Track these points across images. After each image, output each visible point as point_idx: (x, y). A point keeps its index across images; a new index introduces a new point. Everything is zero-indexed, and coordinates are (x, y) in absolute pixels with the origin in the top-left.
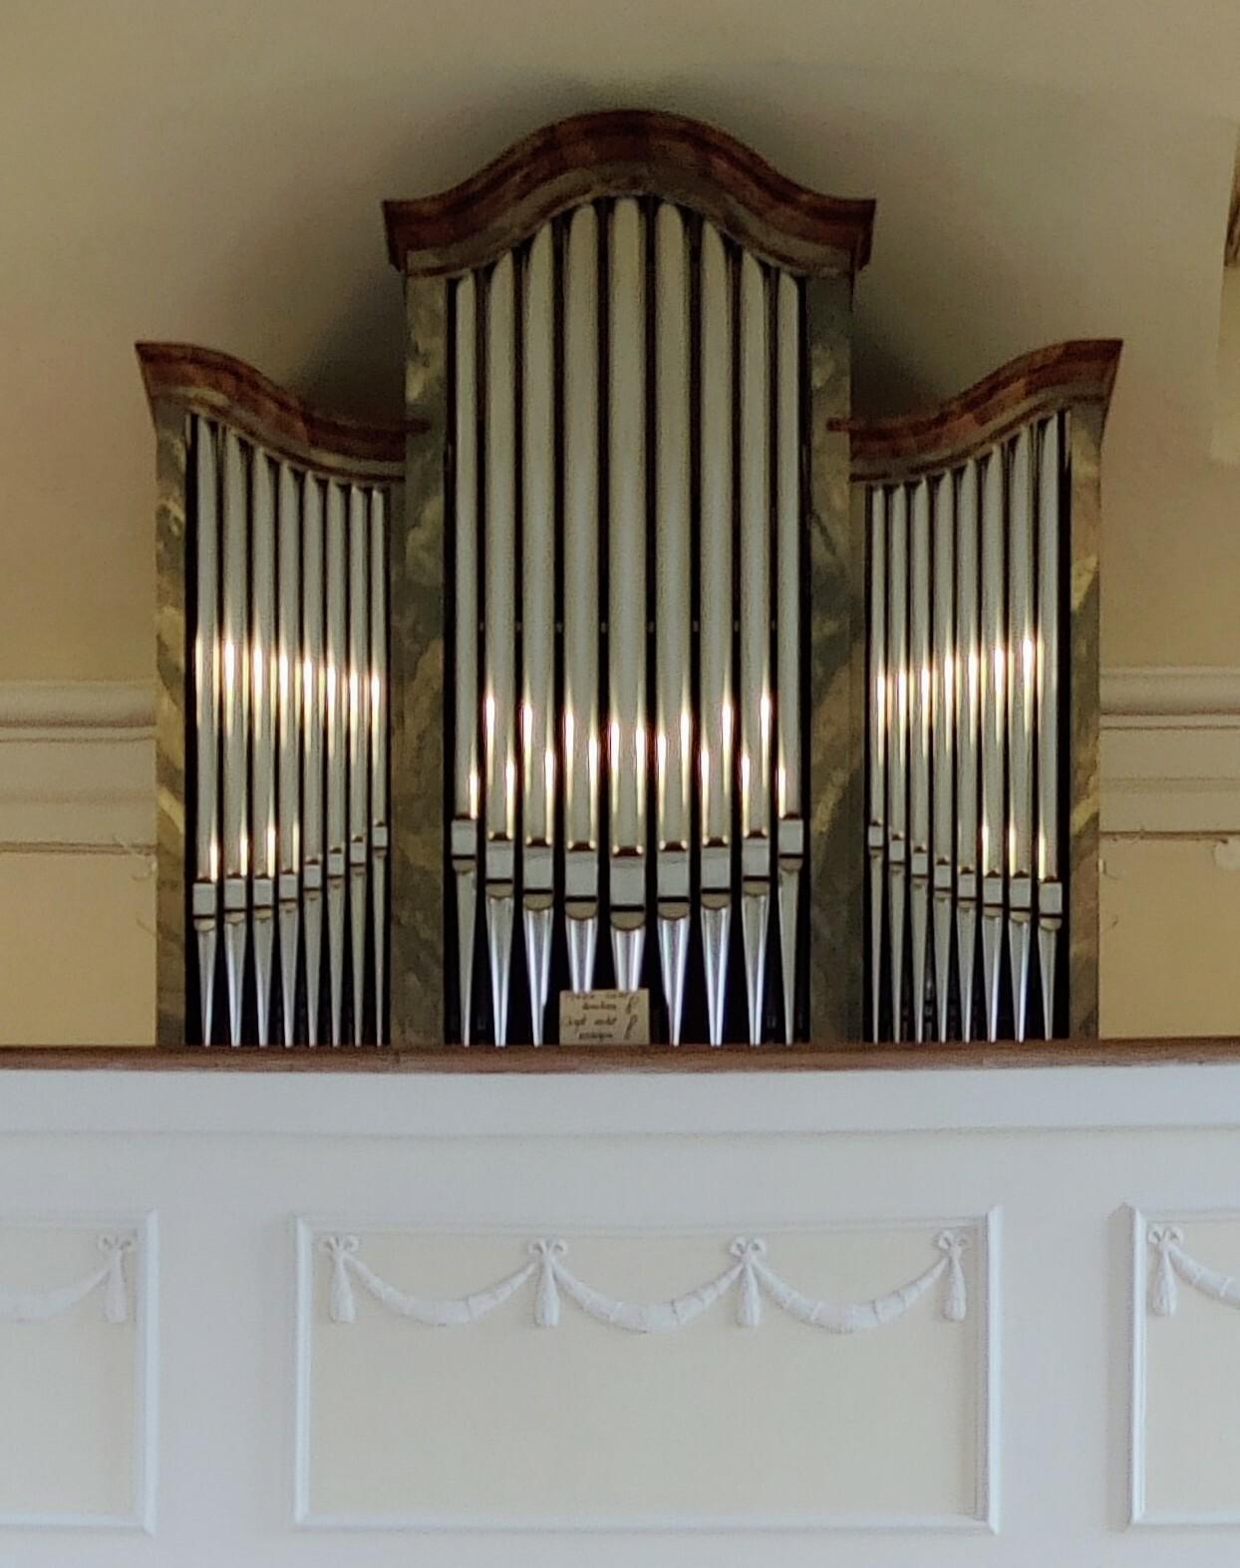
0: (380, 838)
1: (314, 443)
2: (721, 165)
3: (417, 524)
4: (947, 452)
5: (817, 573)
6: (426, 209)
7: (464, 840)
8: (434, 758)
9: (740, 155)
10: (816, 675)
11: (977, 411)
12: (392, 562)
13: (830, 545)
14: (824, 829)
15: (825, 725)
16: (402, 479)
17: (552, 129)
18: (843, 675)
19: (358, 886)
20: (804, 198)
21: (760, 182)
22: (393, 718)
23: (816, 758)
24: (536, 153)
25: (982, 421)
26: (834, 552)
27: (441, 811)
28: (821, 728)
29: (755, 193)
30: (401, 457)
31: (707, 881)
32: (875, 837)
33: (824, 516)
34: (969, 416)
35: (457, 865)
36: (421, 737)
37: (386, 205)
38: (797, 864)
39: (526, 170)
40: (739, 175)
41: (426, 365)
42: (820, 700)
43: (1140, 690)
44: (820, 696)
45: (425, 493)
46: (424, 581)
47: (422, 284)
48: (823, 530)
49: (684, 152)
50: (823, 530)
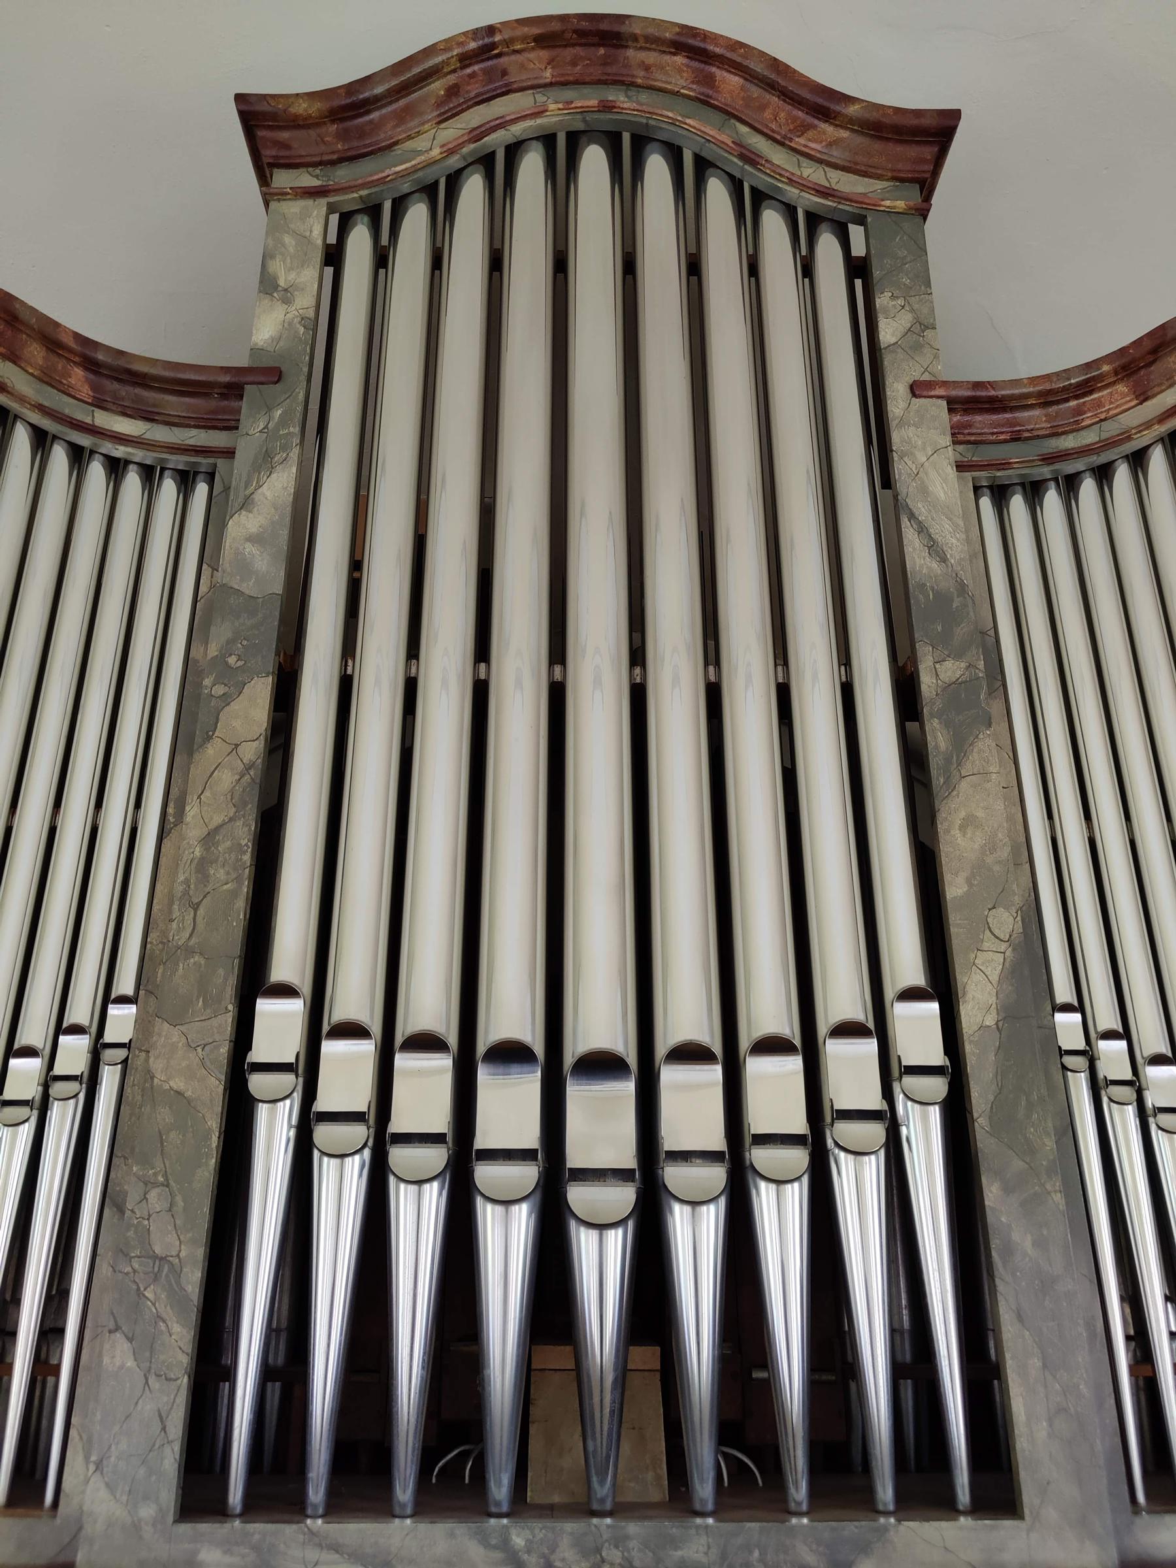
0: (122, 1021)
1: (99, 404)
2: (730, 82)
3: (247, 504)
4: (1089, 437)
5: (245, 804)
6: (300, 108)
7: (279, 1026)
8: (232, 882)
9: (758, 67)
10: (937, 747)
11: (1135, 377)
12: (205, 566)
13: (934, 549)
14: (990, 1021)
15: (963, 828)
16: (230, 453)
17: (491, 30)
18: (985, 746)
19: (62, 1120)
20: (852, 110)
21: (786, 95)
22: (170, 810)
23: (954, 888)
24: (466, 59)
25: (1143, 397)
26: (943, 560)
27: (233, 981)
28: (956, 832)
29: (778, 113)
30: (232, 426)
31: (759, 1120)
32: (1068, 1026)
33: (921, 509)
34: (1121, 388)
35: (258, 1083)
36: (209, 839)
37: (240, 98)
38: (938, 1087)
39: (452, 79)
40: (755, 91)
41: (287, 301)
42: (951, 787)
43: (255, 744)
44: (948, 780)
45: (266, 462)
46: (248, 587)
47: (293, 208)
48: (922, 529)
49: (676, 72)
50: (922, 529)
